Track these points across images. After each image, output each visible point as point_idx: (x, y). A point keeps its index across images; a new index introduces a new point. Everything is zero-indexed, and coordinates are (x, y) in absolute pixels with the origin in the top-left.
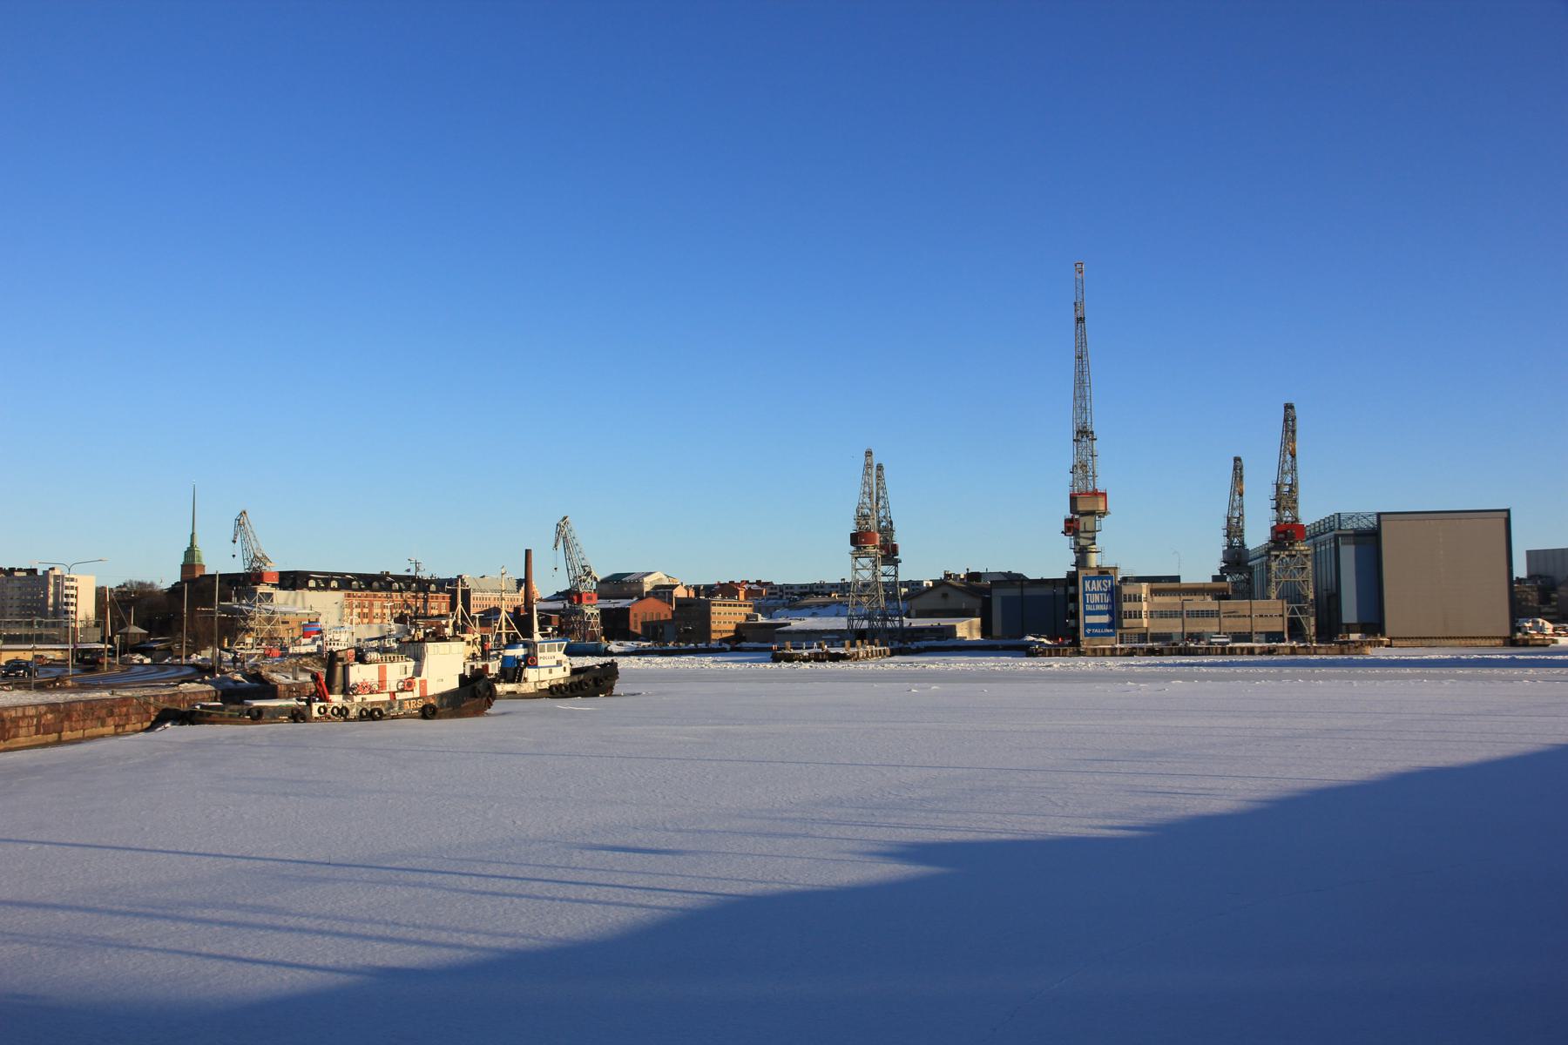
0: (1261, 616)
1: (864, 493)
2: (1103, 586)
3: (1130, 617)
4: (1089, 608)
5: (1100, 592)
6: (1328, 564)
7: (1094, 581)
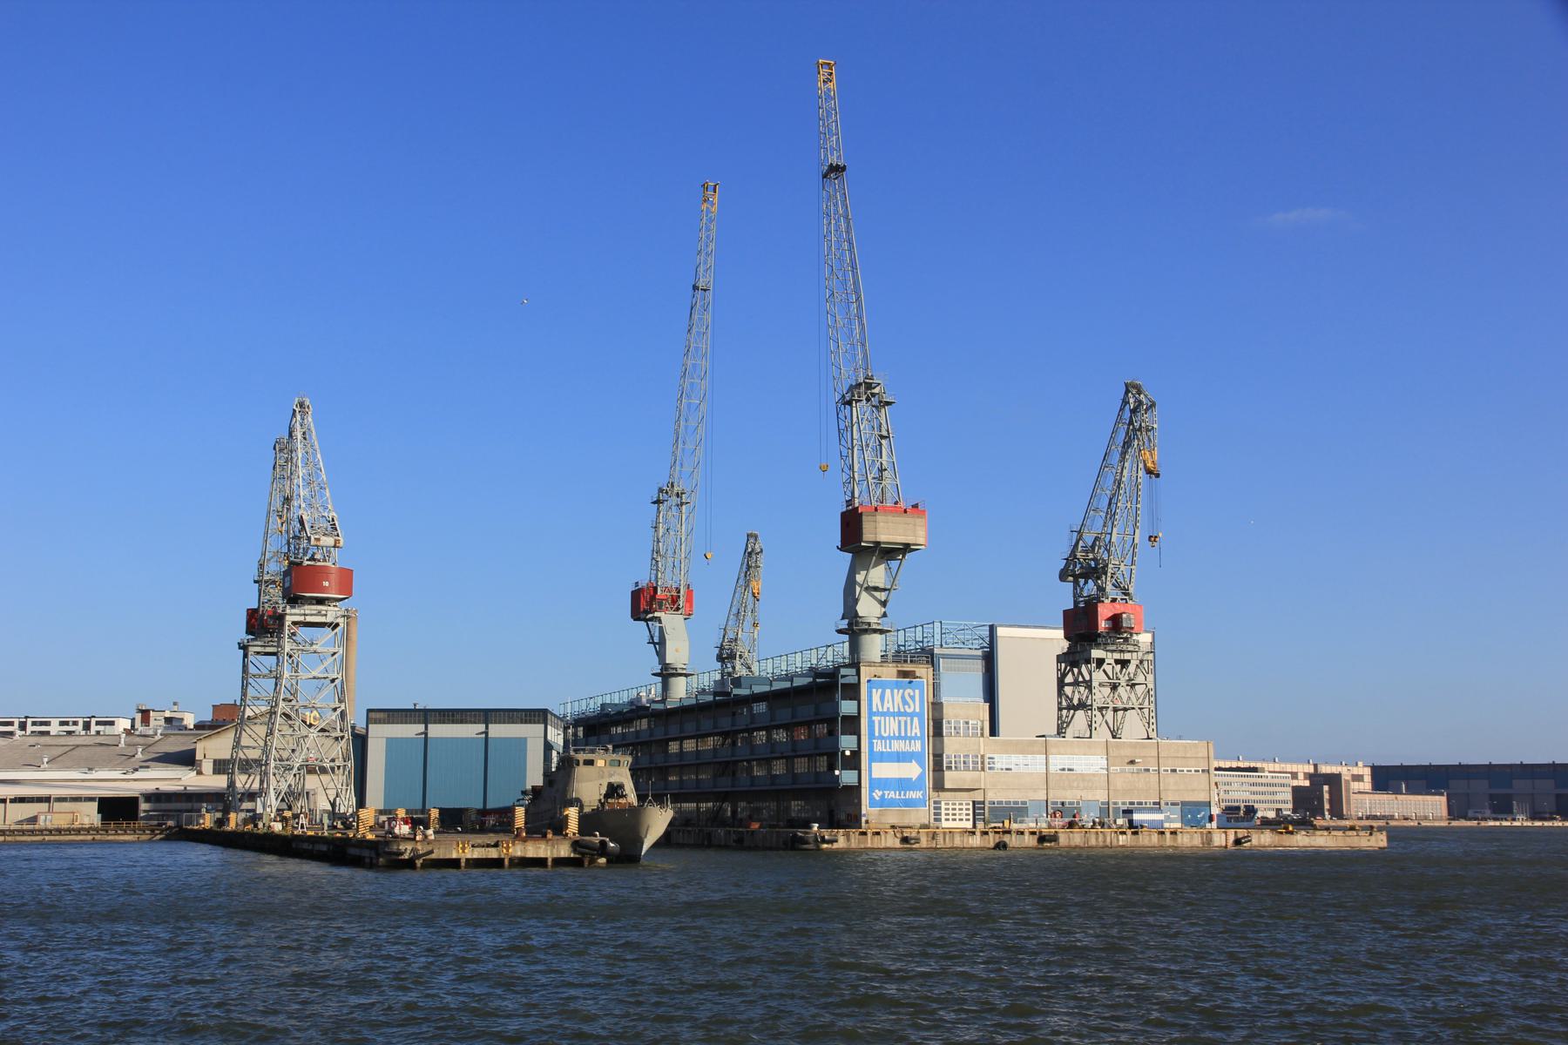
0: (1174, 771)
2: (905, 702)
4: (879, 746)
5: (900, 714)
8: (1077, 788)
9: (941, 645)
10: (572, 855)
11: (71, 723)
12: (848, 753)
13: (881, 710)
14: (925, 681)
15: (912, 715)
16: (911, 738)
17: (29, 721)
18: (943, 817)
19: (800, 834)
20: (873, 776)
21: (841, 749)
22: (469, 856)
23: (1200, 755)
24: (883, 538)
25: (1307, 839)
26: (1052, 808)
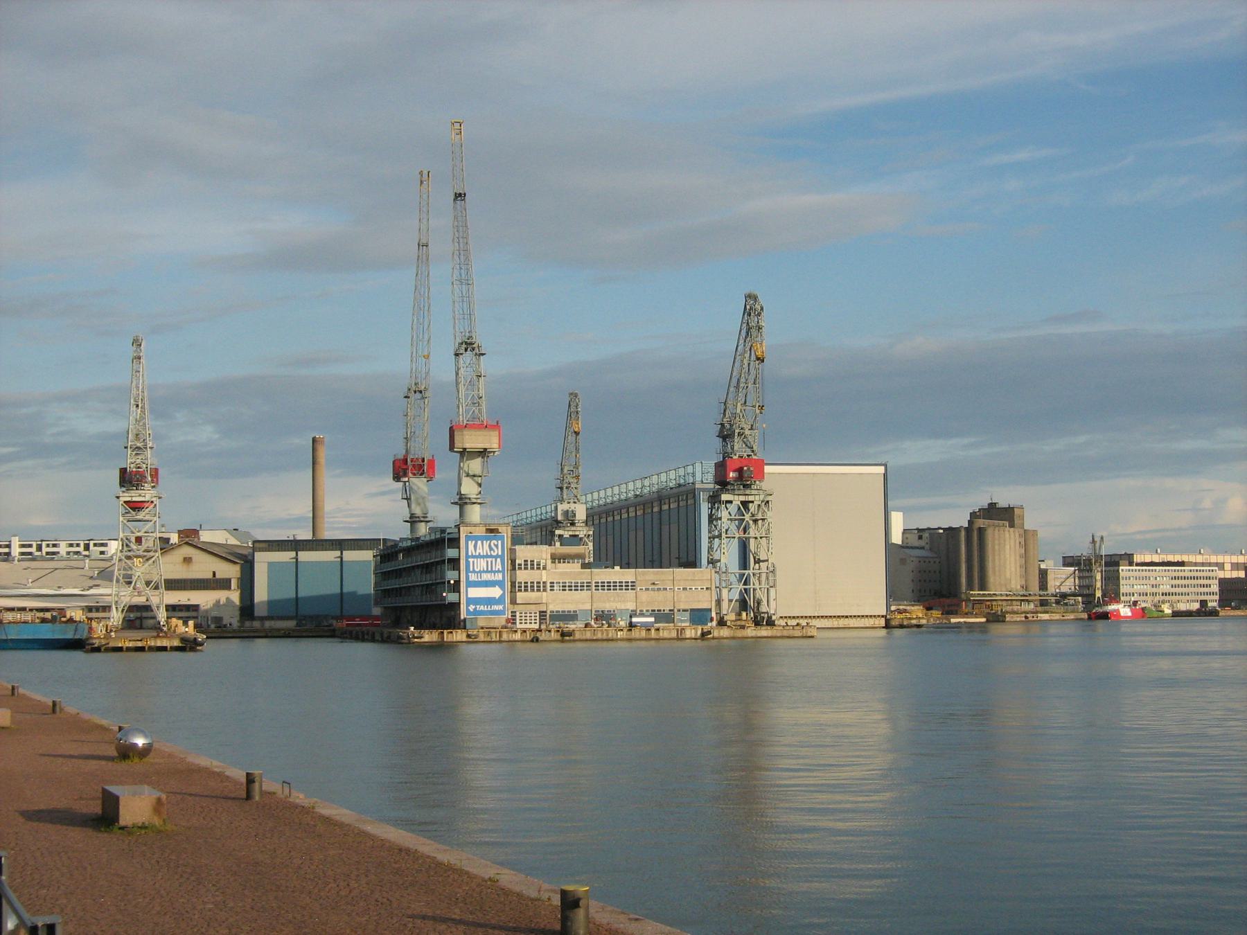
1: (759, 314)
2: (491, 549)
3: (526, 590)
4: (473, 577)
5: (487, 556)
6: (648, 531)
7: (479, 542)
8: (614, 601)
9: (702, 481)
10: (180, 645)
11: (75, 545)
12: (452, 582)
13: (474, 554)
14: (505, 535)
15: (496, 557)
16: (495, 572)
17: (44, 544)
18: (518, 621)
19: (401, 634)
20: (469, 596)
21: (447, 580)
22: (127, 645)
23: (705, 578)
24: (467, 445)
25: (754, 632)
26: (595, 615)
